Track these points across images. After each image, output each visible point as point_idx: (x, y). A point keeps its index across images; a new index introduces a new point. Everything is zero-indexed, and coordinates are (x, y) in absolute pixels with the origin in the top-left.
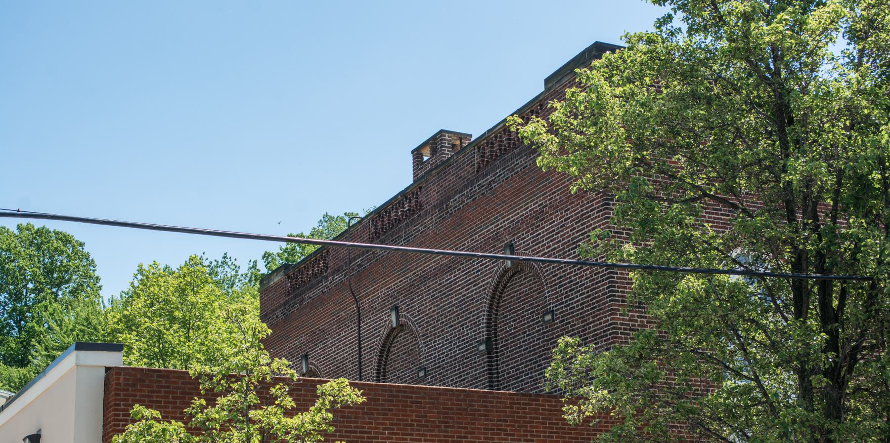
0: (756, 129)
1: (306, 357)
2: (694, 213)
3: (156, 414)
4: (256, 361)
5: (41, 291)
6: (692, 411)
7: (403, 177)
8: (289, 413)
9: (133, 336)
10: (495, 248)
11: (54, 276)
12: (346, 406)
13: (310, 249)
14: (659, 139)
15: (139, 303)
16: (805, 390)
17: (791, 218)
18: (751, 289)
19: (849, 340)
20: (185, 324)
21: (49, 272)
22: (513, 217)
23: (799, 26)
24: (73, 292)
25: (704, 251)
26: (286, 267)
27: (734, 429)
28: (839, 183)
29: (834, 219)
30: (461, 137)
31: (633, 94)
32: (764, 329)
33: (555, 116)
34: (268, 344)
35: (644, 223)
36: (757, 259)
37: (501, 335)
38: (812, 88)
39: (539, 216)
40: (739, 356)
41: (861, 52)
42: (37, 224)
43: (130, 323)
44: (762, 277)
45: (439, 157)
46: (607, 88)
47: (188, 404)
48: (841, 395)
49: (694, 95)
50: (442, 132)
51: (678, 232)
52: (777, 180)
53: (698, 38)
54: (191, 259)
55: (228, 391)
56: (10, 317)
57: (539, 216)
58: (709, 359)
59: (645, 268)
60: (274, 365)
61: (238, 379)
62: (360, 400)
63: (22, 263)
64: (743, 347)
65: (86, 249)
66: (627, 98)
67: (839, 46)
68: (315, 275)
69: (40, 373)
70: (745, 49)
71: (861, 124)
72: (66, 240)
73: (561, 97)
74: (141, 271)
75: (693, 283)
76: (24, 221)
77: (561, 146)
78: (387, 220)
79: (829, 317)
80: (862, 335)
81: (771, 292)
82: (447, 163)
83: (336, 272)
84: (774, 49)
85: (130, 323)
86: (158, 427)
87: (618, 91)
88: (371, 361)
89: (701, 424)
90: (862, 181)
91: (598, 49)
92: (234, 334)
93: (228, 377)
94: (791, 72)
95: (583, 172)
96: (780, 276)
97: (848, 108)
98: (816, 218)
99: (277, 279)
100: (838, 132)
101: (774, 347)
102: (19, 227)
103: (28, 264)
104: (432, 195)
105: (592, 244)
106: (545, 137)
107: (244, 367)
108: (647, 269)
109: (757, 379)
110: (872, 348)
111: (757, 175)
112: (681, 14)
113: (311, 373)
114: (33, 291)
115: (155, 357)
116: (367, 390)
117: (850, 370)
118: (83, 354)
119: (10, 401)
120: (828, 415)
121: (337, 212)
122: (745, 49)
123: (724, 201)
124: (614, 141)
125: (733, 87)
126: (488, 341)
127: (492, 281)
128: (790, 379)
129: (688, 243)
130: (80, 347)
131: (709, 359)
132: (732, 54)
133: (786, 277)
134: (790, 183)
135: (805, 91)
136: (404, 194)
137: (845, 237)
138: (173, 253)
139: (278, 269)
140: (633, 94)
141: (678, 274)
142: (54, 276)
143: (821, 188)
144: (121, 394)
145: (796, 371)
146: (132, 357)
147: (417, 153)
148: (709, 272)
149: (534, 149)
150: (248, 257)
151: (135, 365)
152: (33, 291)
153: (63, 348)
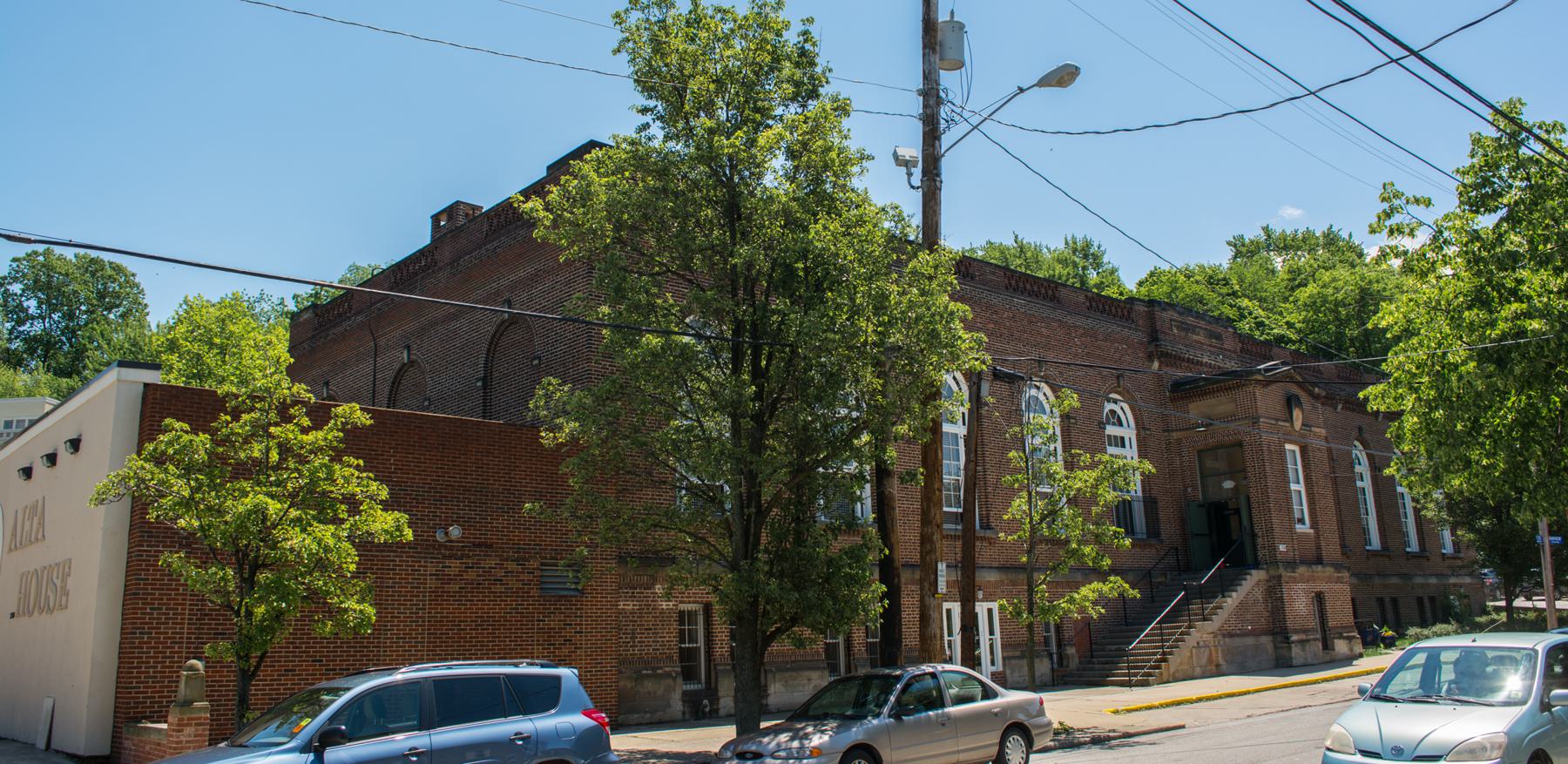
0: (711, 221)
1: (327, 384)
2: (659, 286)
3: (186, 426)
4: (279, 383)
5: (93, 312)
6: (645, 444)
7: (422, 237)
8: (305, 431)
9: (174, 358)
10: (495, 303)
11: (106, 299)
12: (355, 426)
13: (338, 293)
14: (627, 232)
15: (182, 329)
16: (736, 430)
17: (735, 295)
18: (699, 348)
19: (771, 393)
20: (223, 351)
21: (101, 296)
22: (512, 277)
23: (751, 143)
24: (123, 316)
25: (664, 316)
26: (314, 306)
27: (678, 460)
28: (773, 269)
29: (767, 297)
30: (475, 208)
31: (615, 184)
32: (708, 381)
33: (550, 197)
34: (293, 372)
35: (618, 290)
36: (705, 324)
37: (496, 374)
38: (758, 192)
39: (534, 279)
40: (685, 402)
41: (796, 168)
42: (93, 254)
43: (173, 346)
44: (708, 339)
45: (456, 225)
46: (593, 175)
47: (215, 419)
48: (763, 436)
49: (665, 190)
50: (458, 203)
51: (643, 298)
52: (726, 262)
53: (671, 144)
54: (1152, 274)
55: (252, 409)
56: (63, 333)
57: (534, 279)
58: (662, 403)
59: (616, 326)
60: (295, 389)
61: (262, 399)
62: (369, 422)
63: (77, 287)
64: (689, 394)
65: (137, 280)
66: (611, 186)
67: (779, 162)
68: (340, 315)
69: (86, 382)
70: (708, 156)
71: (792, 223)
72: (118, 269)
73: (557, 183)
74: (186, 302)
75: (653, 341)
76: (82, 251)
77: (554, 220)
78: (405, 273)
79: (758, 374)
80: (782, 389)
81: (715, 352)
82: (460, 229)
83: (358, 313)
84: (730, 159)
85: (173, 346)
86: (186, 437)
87: (604, 180)
88: (384, 390)
89: (653, 454)
90: (790, 271)
91: (592, 145)
92: (266, 358)
93: (252, 397)
94: (742, 178)
95: (572, 244)
96: (723, 339)
97: (784, 210)
98: (753, 296)
99: (306, 316)
100: (776, 230)
101: (713, 394)
102: (76, 256)
103: (84, 291)
104: (446, 254)
105: (575, 302)
106: (542, 214)
107: (267, 390)
108: (616, 328)
109: (698, 420)
110: (789, 400)
111: (711, 257)
112: (658, 123)
113: (330, 398)
114: (86, 312)
115: (194, 376)
116: (375, 414)
117: (771, 417)
118: (124, 370)
119: (56, 408)
120: (752, 451)
121: (363, 264)
122: (708, 156)
123: (683, 277)
124: (597, 219)
125: (695, 185)
126: (484, 379)
127: (491, 329)
128: (727, 422)
129: (652, 307)
130: (122, 364)
131: (662, 403)
132: (700, 159)
133: (727, 340)
134: (735, 266)
135: (752, 194)
136: (422, 252)
137: (774, 312)
138: (215, 289)
139: (307, 309)
140: (615, 184)
141: (641, 333)
142: (106, 299)
143: (759, 272)
144: (156, 407)
145: (730, 415)
146: (171, 376)
147: (436, 219)
148: (667, 333)
149: (532, 223)
150: (289, 296)
151: (173, 383)
152: (86, 312)
153: (108, 364)
